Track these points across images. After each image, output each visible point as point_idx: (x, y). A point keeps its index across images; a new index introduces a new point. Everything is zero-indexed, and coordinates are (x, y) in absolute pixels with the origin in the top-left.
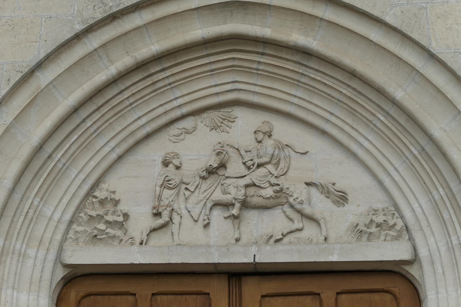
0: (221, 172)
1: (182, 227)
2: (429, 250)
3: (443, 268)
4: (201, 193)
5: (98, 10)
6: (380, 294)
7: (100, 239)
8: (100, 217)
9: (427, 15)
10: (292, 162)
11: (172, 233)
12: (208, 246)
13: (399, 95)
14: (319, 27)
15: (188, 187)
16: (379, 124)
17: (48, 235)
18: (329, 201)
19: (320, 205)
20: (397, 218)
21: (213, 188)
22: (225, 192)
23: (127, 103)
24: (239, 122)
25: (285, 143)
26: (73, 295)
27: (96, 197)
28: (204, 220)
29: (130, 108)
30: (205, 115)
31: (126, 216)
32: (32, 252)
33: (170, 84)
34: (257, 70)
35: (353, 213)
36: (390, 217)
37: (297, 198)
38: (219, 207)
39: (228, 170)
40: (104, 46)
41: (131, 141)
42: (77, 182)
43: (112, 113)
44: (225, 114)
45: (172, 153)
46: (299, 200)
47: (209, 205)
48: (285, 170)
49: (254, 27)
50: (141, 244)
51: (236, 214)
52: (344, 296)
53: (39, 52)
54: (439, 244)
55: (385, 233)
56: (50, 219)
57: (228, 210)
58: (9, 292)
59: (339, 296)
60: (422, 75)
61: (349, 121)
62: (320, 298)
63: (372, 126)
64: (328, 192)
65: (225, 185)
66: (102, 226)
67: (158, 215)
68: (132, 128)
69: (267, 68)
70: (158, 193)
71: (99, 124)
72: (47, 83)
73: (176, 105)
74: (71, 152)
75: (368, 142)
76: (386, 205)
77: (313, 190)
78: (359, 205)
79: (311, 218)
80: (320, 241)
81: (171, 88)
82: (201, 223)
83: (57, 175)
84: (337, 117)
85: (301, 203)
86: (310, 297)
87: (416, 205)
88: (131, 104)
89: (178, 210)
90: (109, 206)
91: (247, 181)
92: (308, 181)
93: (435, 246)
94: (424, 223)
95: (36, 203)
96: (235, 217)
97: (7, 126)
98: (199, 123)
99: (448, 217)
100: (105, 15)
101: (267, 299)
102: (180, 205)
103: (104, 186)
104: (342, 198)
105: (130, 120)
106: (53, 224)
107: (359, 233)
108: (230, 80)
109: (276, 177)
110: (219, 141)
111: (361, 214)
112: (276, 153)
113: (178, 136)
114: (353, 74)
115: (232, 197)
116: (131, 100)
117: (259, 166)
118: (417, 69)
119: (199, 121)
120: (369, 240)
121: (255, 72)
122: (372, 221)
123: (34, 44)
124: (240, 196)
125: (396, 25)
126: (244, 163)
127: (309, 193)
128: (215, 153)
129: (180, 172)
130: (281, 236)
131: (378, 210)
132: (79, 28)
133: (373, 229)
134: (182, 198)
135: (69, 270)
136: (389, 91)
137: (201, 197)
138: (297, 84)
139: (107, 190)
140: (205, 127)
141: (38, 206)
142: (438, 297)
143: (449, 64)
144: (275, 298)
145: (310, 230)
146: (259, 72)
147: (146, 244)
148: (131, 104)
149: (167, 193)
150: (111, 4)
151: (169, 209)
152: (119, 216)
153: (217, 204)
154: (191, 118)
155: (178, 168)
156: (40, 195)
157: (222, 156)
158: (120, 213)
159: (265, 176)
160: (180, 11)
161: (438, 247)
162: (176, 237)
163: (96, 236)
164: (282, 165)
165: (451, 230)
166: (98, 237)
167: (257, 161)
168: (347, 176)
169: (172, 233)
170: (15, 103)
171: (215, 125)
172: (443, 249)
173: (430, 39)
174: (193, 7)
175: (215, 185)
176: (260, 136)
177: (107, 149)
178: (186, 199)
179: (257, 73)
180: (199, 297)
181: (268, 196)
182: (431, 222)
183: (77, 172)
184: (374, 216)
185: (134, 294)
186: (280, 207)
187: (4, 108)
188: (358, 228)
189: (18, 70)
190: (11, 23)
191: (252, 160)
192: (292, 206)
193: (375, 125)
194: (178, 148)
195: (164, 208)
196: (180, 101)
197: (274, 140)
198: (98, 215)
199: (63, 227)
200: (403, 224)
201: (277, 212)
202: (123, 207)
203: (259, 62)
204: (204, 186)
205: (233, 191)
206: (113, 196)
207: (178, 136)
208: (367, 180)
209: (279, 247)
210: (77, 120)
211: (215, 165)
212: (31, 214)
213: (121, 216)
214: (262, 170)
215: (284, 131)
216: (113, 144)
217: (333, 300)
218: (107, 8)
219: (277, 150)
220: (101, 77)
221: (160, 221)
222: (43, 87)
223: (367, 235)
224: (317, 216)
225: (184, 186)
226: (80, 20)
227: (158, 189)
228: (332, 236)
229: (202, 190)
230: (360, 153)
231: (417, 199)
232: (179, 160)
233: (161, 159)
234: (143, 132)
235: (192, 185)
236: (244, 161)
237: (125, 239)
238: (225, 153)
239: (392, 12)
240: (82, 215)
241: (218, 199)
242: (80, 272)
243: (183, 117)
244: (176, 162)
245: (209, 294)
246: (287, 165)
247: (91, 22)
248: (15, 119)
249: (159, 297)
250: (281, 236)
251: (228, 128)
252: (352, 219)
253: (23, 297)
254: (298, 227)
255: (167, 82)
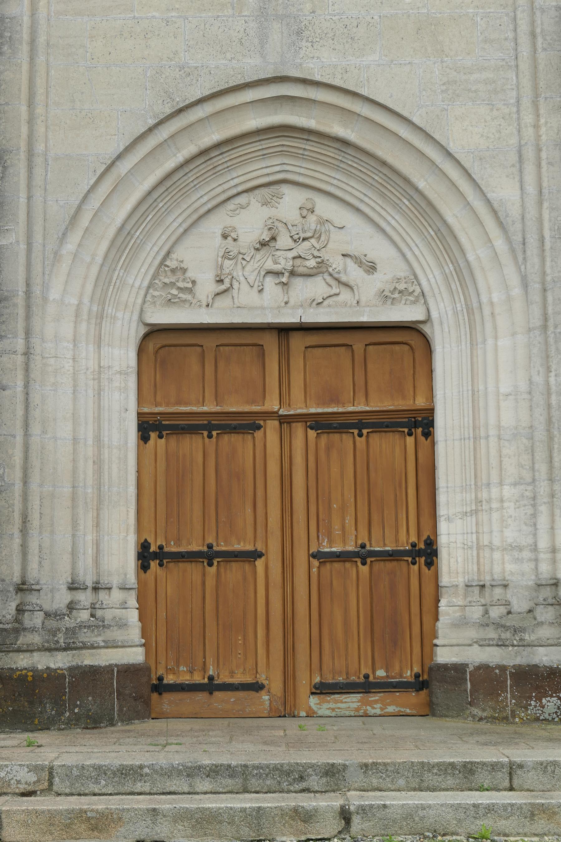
0: (272, 244)
1: (240, 292)
2: (439, 313)
3: (449, 328)
4: (255, 263)
5: (167, 106)
6: (400, 345)
7: (174, 302)
8: (173, 284)
9: (447, 116)
10: (331, 235)
11: (233, 297)
12: (263, 308)
13: (421, 185)
14: (357, 121)
15: (245, 257)
16: (404, 208)
17: (132, 300)
18: (361, 270)
19: (354, 274)
20: (416, 285)
21: (266, 258)
22: (276, 263)
23: (192, 185)
24: (286, 198)
25: (325, 219)
26: (151, 346)
27: (168, 267)
28: (259, 286)
29: (194, 189)
30: (257, 192)
31: (194, 282)
32: (120, 315)
33: (228, 167)
34: (303, 155)
35: (379, 281)
36: (410, 285)
37: (335, 269)
38: (270, 274)
39: (278, 243)
40: (172, 137)
41: (195, 216)
42: (152, 254)
43: (179, 194)
44: (274, 191)
45: (230, 227)
46: (337, 270)
47: (263, 273)
48: (326, 242)
49: (301, 118)
50: (208, 306)
51: (285, 282)
52: (371, 347)
53: (118, 145)
54: (447, 309)
55: (405, 298)
56: (132, 286)
57: (279, 277)
58: (106, 348)
59: (367, 347)
60: (440, 169)
61: (380, 202)
62: (352, 349)
63: (399, 208)
64: (361, 262)
65: (276, 256)
66: (175, 292)
67: (221, 281)
68: (196, 205)
69: (311, 154)
70: (220, 263)
71: (169, 204)
72: (127, 171)
73: (233, 185)
74: (147, 229)
75: (394, 220)
76: (407, 274)
77: (348, 260)
78: (385, 274)
79: (346, 285)
80: (354, 304)
81: (229, 170)
82: (256, 289)
83: (136, 249)
84: (370, 198)
85: (339, 273)
86: (344, 347)
87: (431, 276)
88: (195, 186)
89: (237, 277)
90: (179, 274)
91: (294, 253)
92: (344, 253)
93: (444, 310)
94: (436, 291)
95: (121, 274)
96: (284, 284)
97: (95, 211)
98: (252, 199)
99: (455, 288)
100: (174, 110)
101: (309, 349)
102: (238, 273)
103: (174, 256)
104: (371, 268)
105: (194, 198)
106: (135, 290)
107: (385, 298)
108: (279, 163)
109: (318, 250)
110: (269, 216)
111: (387, 282)
112: (318, 228)
113: (234, 211)
114: (384, 163)
115: (282, 267)
116: (195, 183)
117: (304, 239)
118: (437, 164)
119: (252, 197)
120: (392, 304)
121: (301, 156)
122: (395, 288)
123: (113, 137)
124: (289, 267)
125: (421, 126)
126: (291, 237)
127: (345, 264)
128: (266, 228)
129: (238, 243)
130: (322, 300)
131: (401, 279)
132: (151, 122)
133: (396, 295)
134: (239, 266)
135: (149, 328)
136: (413, 181)
137: (256, 266)
138: (337, 168)
139: (177, 260)
140: (257, 203)
141: (123, 276)
142: (443, 351)
143: (462, 163)
144: (316, 349)
145: (345, 296)
146: (304, 157)
147: (211, 307)
148: (195, 186)
149: (227, 263)
150: (178, 100)
151: (229, 277)
152: (188, 282)
153: (269, 272)
154: (246, 195)
155: (235, 240)
156: (124, 267)
157: (273, 231)
158: (189, 280)
159: (310, 249)
160: (237, 104)
161: (446, 311)
162: (236, 300)
163: (170, 300)
164: (323, 238)
165: (456, 298)
166: (172, 301)
167: (302, 235)
168: (377, 249)
169: (233, 297)
170: (100, 190)
171: (266, 201)
172: (450, 313)
173: (448, 139)
174: (249, 101)
175: (267, 256)
176: (305, 212)
177: (176, 224)
178: (243, 268)
179: (303, 158)
180: (254, 348)
181: (312, 266)
182: (442, 290)
183: (151, 245)
184: (398, 284)
185: (202, 346)
186: (321, 275)
187: (91, 195)
188: (384, 293)
189: (101, 161)
190: (90, 115)
191: (297, 234)
192: (331, 275)
193: (401, 208)
194: (235, 221)
195: (225, 276)
196: (236, 181)
197: (317, 216)
198: (171, 282)
199: (142, 293)
200: (420, 291)
201: (319, 279)
202: (189, 274)
203: (305, 149)
204: (258, 256)
205: (283, 262)
206: (182, 265)
207: (234, 211)
208: (392, 252)
209: (321, 310)
210: (150, 201)
211: (267, 239)
212: (118, 284)
213: (190, 283)
214: (306, 243)
215: (325, 207)
216: (180, 220)
217: (363, 351)
218: (175, 103)
219: (319, 225)
220: (170, 165)
221: (222, 287)
222: (122, 176)
223: (391, 300)
224: (352, 283)
225: (241, 256)
226: (152, 114)
227: (220, 259)
228: (363, 300)
229: (256, 261)
230: (388, 229)
231: (432, 271)
232: (236, 233)
233: (220, 232)
234: (206, 208)
235: (248, 256)
236: (291, 235)
237: (194, 301)
238: (275, 228)
239: (418, 113)
240: (157, 281)
241: (270, 268)
242: (156, 328)
243: (238, 194)
244: (234, 235)
245: (263, 345)
246: (327, 238)
247: (162, 117)
248: (101, 204)
249: (221, 348)
250: (322, 300)
251: (277, 204)
252: (379, 285)
253: (116, 352)
254: (335, 293)
255: (225, 165)
